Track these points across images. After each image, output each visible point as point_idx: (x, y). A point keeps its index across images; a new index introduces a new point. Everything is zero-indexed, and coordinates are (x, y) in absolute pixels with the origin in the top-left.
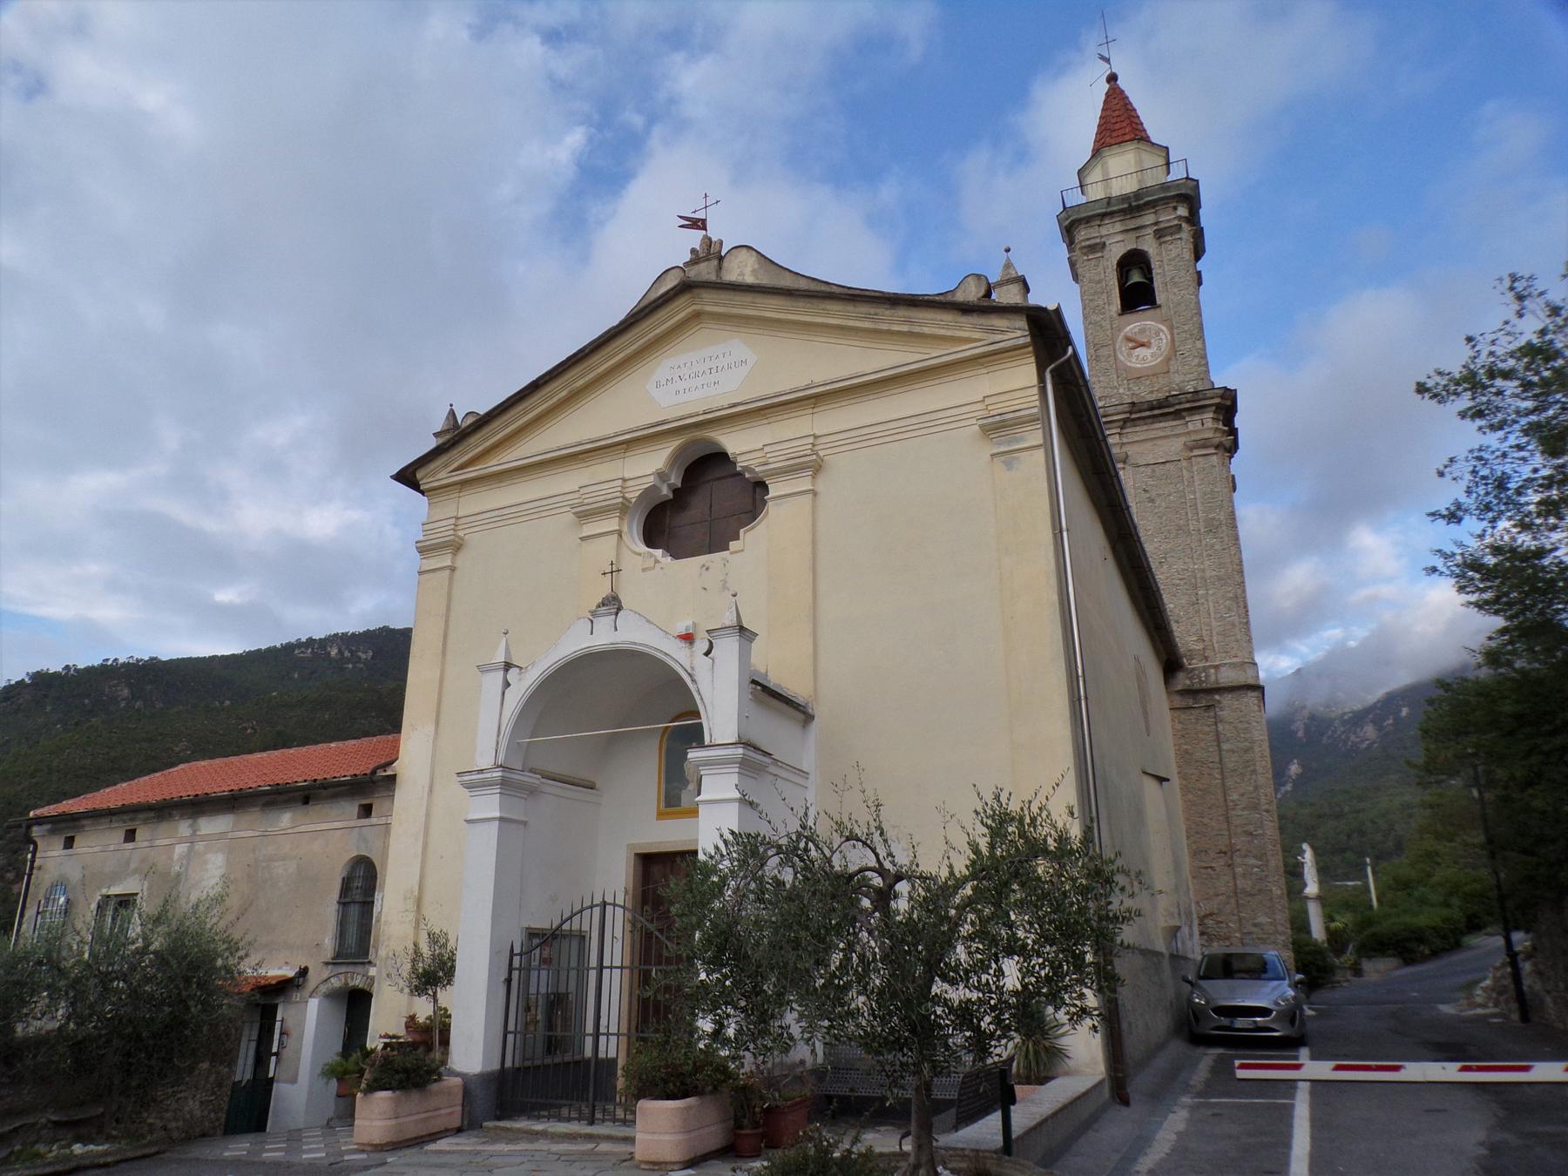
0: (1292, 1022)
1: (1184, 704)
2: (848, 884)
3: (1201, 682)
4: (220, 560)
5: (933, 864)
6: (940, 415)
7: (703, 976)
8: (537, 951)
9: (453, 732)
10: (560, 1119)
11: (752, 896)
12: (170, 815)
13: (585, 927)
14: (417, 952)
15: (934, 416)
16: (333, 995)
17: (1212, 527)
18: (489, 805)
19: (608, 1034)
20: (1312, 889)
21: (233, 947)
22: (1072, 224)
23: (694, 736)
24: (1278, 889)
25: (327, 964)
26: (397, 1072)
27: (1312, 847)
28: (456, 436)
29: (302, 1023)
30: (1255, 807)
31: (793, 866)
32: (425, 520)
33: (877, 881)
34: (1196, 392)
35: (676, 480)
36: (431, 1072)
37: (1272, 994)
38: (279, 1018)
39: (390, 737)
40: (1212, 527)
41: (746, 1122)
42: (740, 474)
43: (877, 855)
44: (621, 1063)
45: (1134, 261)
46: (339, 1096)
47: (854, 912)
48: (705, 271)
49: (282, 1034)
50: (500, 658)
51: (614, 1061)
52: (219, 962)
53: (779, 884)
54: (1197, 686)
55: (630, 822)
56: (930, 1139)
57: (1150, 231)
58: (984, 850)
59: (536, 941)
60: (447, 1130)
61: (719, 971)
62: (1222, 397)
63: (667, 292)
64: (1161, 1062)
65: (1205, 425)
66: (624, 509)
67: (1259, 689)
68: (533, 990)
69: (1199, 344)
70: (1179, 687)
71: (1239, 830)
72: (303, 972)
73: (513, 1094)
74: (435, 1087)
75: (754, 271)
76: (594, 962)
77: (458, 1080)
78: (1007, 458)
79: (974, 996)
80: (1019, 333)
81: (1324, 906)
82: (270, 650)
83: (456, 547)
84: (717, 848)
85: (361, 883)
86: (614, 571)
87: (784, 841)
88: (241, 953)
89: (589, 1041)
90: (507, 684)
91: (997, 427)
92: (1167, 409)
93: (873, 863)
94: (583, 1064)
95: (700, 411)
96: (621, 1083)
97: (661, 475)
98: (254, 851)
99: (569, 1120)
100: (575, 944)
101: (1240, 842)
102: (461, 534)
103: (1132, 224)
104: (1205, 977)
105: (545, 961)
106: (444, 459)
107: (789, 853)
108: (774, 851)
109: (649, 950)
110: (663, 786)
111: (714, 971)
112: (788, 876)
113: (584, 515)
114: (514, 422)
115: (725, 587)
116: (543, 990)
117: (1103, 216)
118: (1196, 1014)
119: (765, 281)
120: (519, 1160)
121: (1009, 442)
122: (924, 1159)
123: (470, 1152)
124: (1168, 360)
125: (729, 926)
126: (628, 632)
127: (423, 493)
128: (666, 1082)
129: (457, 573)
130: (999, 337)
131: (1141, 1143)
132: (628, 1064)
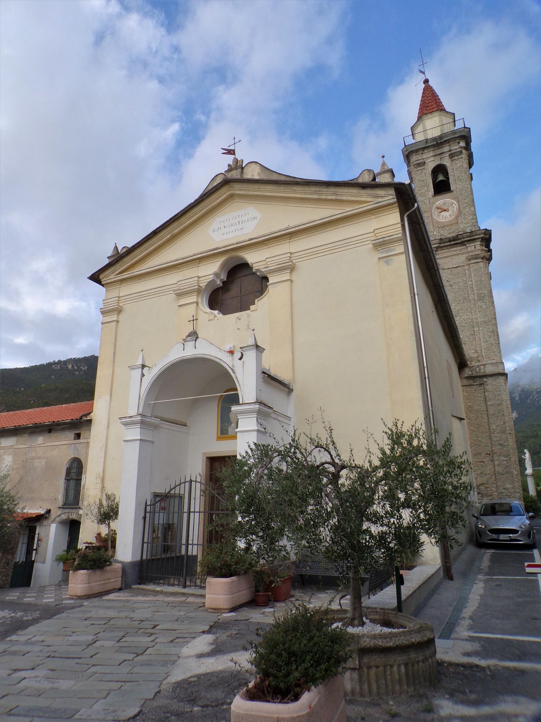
0: (529, 536)
1: (468, 383)
2: (315, 471)
3: (477, 372)
4: (16, 323)
5: (360, 460)
7: (240, 519)
8: (158, 504)
9: (119, 398)
10: (169, 585)
11: (265, 477)
13: (182, 492)
14: (101, 504)
16: (63, 523)
17: (481, 298)
18: (135, 433)
19: (193, 545)
20: (529, 471)
21: (12, 499)
22: (409, 154)
23: (234, 399)
24: (515, 471)
25: (60, 508)
26: (90, 561)
27: (529, 451)
28: (118, 258)
29: (48, 536)
30: (503, 432)
31: (287, 462)
32: (104, 298)
33: (332, 469)
34: (472, 232)
35: (224, 277)
36: (106, 561)
37: (518, 522)
38: (37, 533)
39: (90, 402)
40: (481, 298)
41: (261, 588)
42: (254, 273)
43: (331, 456)
44: (200, 558)
45: (440, 169)
46: (64, 571)
47: (319, 486)
48: (235, 174)
49: (38, 540)
50: (140, 362)
51: (196, 557)
52: (5, 507)
53: (281, 471)
54: (475, 375)
55: (203, 442)
56: (360, 603)
57: (447, 155)
58: (388, 452)
59: (158, 499)
60: (114, 589)
61: (249, 516)
62: (484, 234)
63: (217, 185)
64: (465, 556)
65: (476, 247)
66: (199, 291)
67: (505, 375)
68: (156, 522)
69: (472, 209)
70: (466, 375)
71: (497, 443)
72: (49, 512)
73: (145, 572)
74: (108, 568)
75: (259, 174)
76: (186, 509)
77: (120, 565)
78: (386, 259)
79: (385, 529)
80: (391, 197)
81: (534, 478)
82: (41, 366)
83: (119, 311)
84: (247, 452)
85: (75, 471)
86: (195, 320)
87: (282, 449)
88: (16, 502)
89: (183, 547)
90: (143, 375)
91: (381, 245)
92: (457, 241)
93: (329, 460)
94: (183, 557)
95: (235, 242)
96: (199, 569)
97: (216, 275)
99: (173, 585)
100: (177, 500)
101: (496, 449)
102: (121, 304)
103: (438, 152)
104: (485, 514)
105: (163, 509)
106: (112, 269)
107: (284, 455)
108: (276, 454)
109: (212, 505)
110: (219, 425)
111: (246, 517)
112: (284, 467)
113: (180, 295)
114: (145, 250)
115: (248, 328)
116: (161, 522)
117: (424, 149)
118: (480, 533)
119: (264, 177)
120: (148, 605)
121: (387, 252)
122: (357, 616)
123: (125, 601)
124: (457, 217)
125: (254, 493)
126: (201, 349)
127: (103, 285)
128: (221, 569)
129: (120, 324)
131: (462, 601)
132: (203, 559)
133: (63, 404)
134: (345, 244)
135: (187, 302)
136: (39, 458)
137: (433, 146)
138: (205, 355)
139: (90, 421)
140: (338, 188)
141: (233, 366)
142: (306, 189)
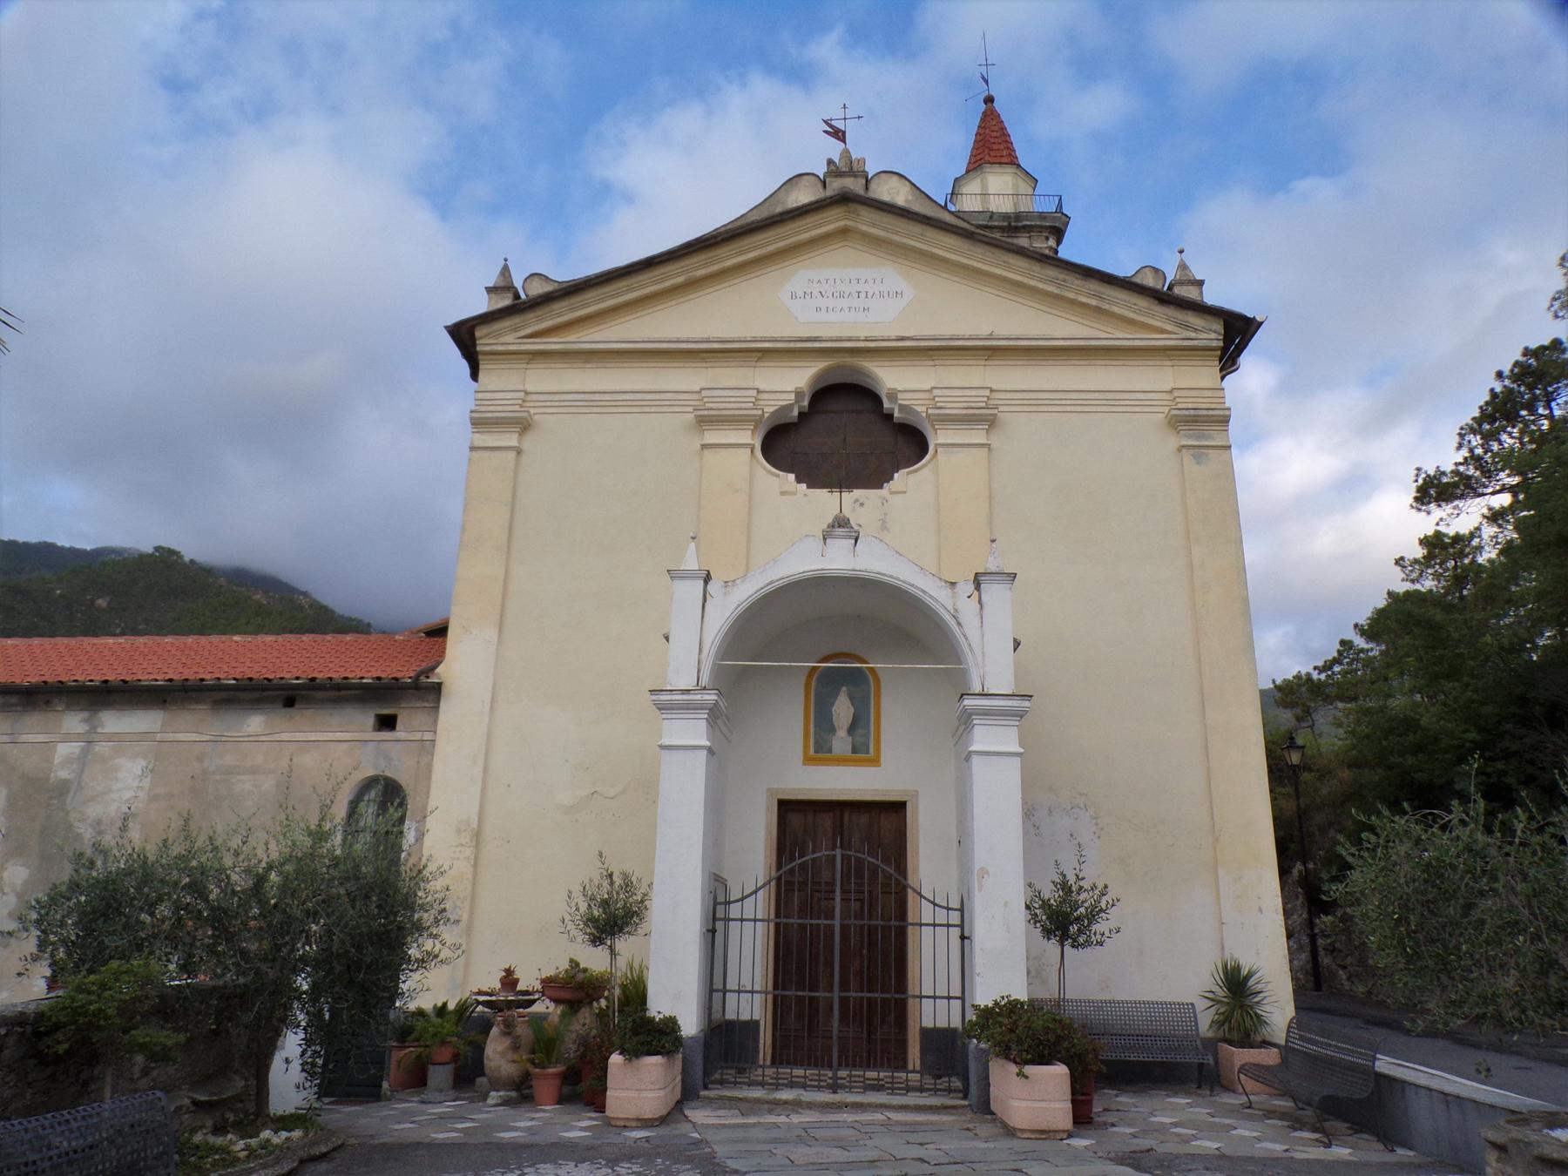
12: (47, 703)
15: (1118, 396)
66: (757, 421)
83: (524, 426)
95: (863, 335)
97: (799, 394)
98: (200, 759)
113: (706, 421)
121: (1198, 438)
130: (1193, 335)
134: (1111, 401)
139: (437, 689)
142: (1037, 268)
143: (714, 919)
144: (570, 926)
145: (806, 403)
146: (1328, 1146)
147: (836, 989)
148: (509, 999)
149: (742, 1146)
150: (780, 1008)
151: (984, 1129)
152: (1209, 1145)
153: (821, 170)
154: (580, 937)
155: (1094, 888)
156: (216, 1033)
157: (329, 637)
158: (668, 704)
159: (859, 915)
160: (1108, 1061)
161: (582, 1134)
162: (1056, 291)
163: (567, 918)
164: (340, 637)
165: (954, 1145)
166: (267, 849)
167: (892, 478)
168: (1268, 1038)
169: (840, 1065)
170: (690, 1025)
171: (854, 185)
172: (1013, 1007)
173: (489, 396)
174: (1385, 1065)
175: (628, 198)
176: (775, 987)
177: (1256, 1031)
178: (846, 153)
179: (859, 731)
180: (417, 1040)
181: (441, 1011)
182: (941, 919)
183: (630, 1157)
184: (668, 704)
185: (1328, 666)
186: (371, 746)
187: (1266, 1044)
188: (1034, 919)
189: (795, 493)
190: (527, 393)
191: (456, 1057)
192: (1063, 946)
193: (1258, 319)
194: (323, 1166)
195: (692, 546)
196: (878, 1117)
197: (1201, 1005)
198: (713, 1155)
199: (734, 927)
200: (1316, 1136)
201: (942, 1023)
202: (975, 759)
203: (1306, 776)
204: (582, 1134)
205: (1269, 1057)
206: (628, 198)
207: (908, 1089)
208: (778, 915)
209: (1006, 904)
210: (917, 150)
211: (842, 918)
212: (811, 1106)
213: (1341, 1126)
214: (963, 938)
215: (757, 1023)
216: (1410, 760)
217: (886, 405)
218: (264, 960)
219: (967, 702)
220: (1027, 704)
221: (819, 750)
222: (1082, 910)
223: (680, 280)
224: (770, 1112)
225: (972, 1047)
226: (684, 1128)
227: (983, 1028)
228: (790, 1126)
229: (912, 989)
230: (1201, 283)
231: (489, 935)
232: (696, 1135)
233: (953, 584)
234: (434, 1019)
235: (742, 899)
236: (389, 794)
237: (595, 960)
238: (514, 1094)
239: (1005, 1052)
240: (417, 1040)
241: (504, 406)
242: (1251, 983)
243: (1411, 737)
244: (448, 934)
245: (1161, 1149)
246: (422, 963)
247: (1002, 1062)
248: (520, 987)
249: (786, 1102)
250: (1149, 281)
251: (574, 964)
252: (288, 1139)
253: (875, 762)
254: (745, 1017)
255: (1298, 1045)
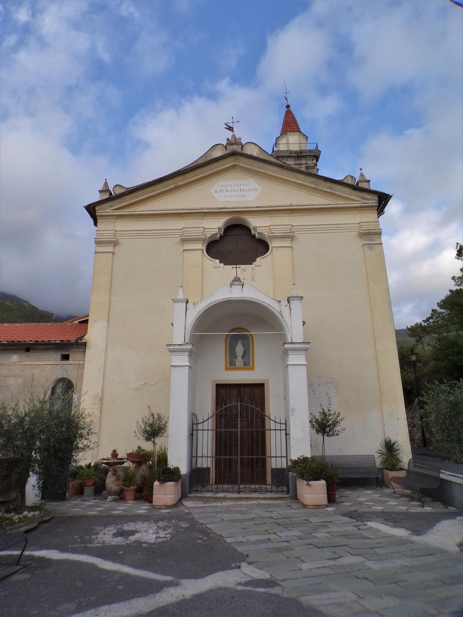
6: (342, 226)
75: (257, 154)
80: (374, 201)
83: (115, 244)
95: (243, 206)
97: (219, 229)
103: (298, 162)
113: (184, 241)
117: (288, 157)
121: (370, 241)
130: (366, 201)
133: (5, 323)
135: (192, 248)
136: (15, 376)
137: (295, 157)
138: (259, 300)
139: (85, 344)
140: (334, 184)
141: (281, 311)
142: (307, 178)
143: (193, 430)
144: (138, 434)
145: (222, 232)
146: (423, 507)
147: (239, 455)
148: (115, 461)
149: (204, 515)
150: (218, 463)
151: (295, 506)
152: (379, 508)
153: (225, 143)
154: (142, 438)
155: (335, 414)
156: (5, 476)
157: (41, 324)
158: (174, 350)
159: (247, 427)
160: (340, 478)
161: (144, 511)
162: (315, 187)
163: (137, 431)
164: (46, 324)
165: (283, 512)
166: (23, 408)
167: (256, 261)
168: (402, 467)
169: (241, 483)
170: (184, 470)
171: (237, 148)
172: (305, 460)
173: (101, 232)
174: (445, 475)
175: (147, 146)
176: (216, 455)
177: (397, 465)
178: (234, 136)
179: (246, 357)
180: (79, 477)
181: (89, 466)
182: (278, 428)
183: (162, 519)
184: (174, 350)
185: (428, 320)
186: (60, 366)
187: (401, 469)
188: (313, 426)
189: (219, 267)
190: (116, 231)
191: (95, 484)
192: (323, 436)
193: (390, 194)
194: (47, 525)
195: (181, 290)
196: (255, 502)
197: (376, 455)
198: (193, 518)
199: (200, 432)
200: (419, 503)
201: (279, 466)
202: (289, 367)
203: (419, 364)
204: (144, 511)
205: (402, 474)
206: (147, 146)
207: (267, 491)
208: (216, 428)
209: (302, 421)
210: (261, 135)
211: (241, 428)
212: (230, 499)
213: (429, 499)
214: (286, 434)
215: (209, 469)
216: (456, 358)
217: (253, 232)
218: (24, 449)
219: (286, 346)
220: (308, 346)
221: (231, 365)
222: (331, 422)
223: (173, 186)
224: (215, 502)
225: (290, 475)
226: (182, 508)
227: (294, 468)
228: (222, 507)
229: (268, 454)
230: (369, 181)
231: (108, 437)
232: (187, 511)
233: (280, 301)
234: (86, 469)
235: (203, 422)
236: (67, 386)
237: (147, 446)
238: (117, 497)
239: (302, 477)
240: (79, 477)
241: (108, 236)
242: (395, 446)
243: (456, 349)
244: (93, 438)
245: (360, 510)
246: (83, 449)
247: (301, 480)
248: (119, 457)
249: (220, 498)
250: (350, 181)
251: (139, 448)
252: (34, 515)
253: (252, 369)
254: (205, 466)
255: (412, 469)
